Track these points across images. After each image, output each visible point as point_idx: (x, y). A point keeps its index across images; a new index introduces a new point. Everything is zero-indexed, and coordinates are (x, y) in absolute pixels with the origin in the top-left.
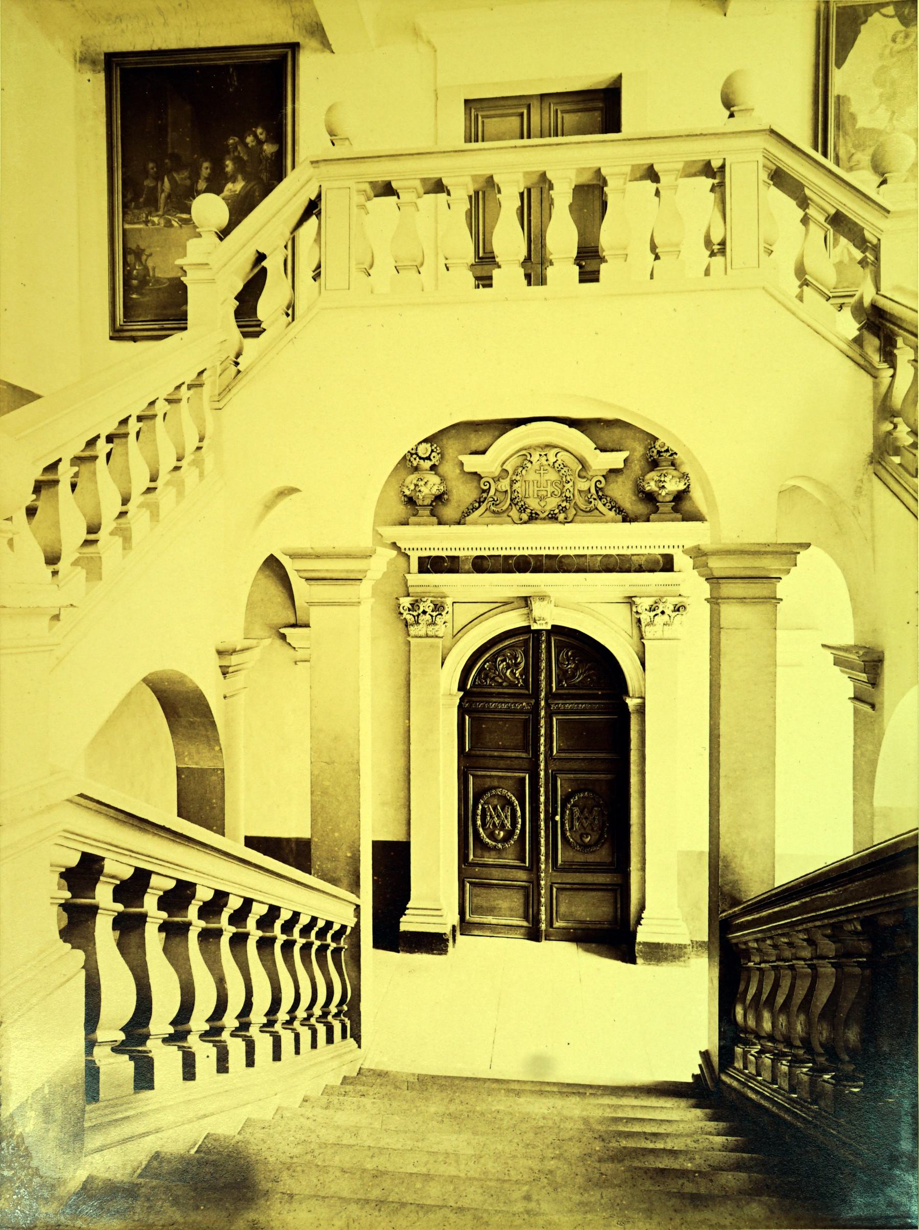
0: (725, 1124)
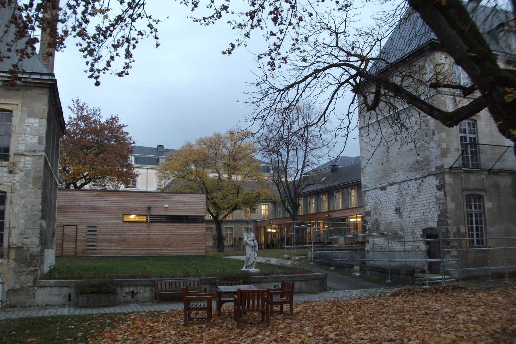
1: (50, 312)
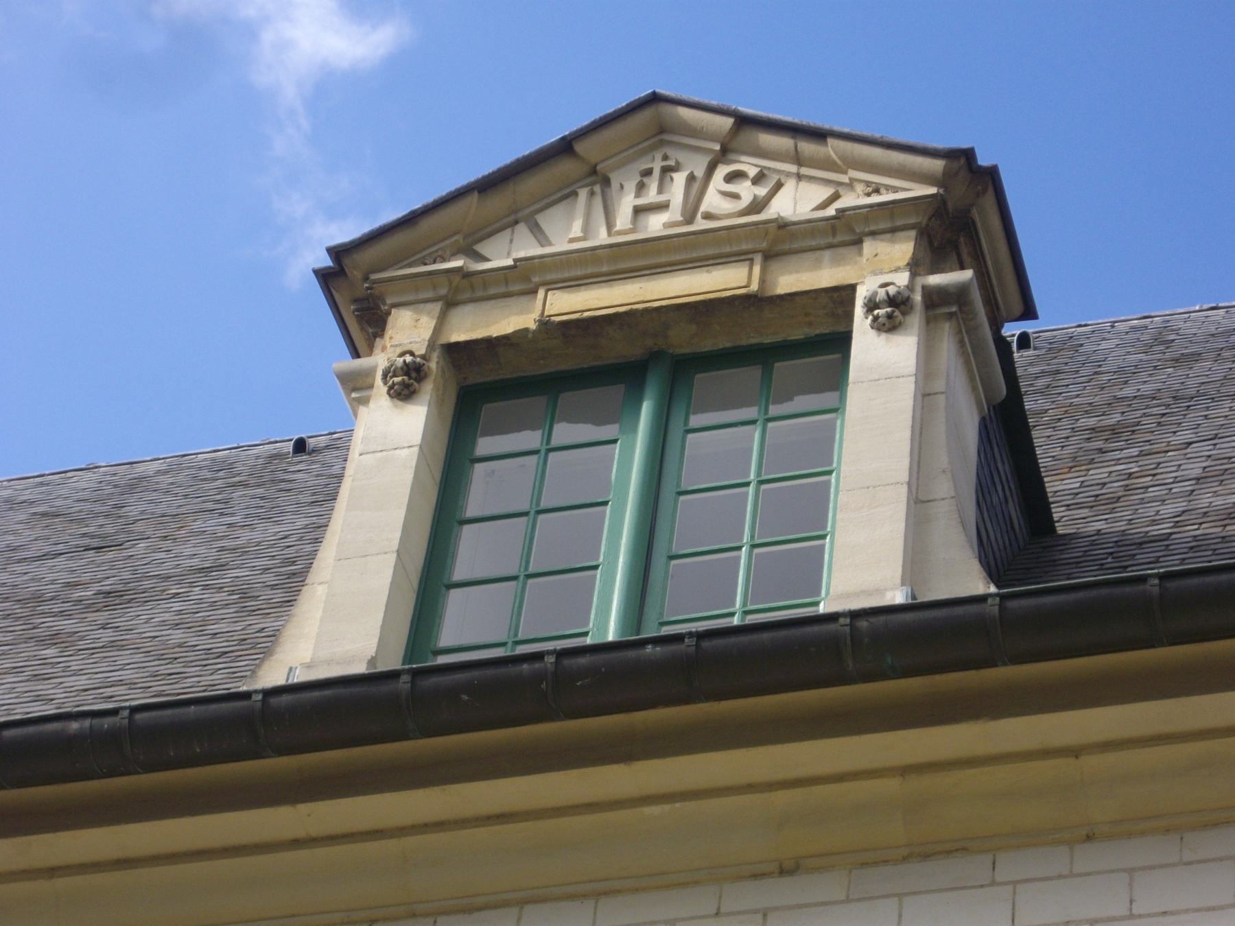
0: (273, 675)
1: (404, 334)
